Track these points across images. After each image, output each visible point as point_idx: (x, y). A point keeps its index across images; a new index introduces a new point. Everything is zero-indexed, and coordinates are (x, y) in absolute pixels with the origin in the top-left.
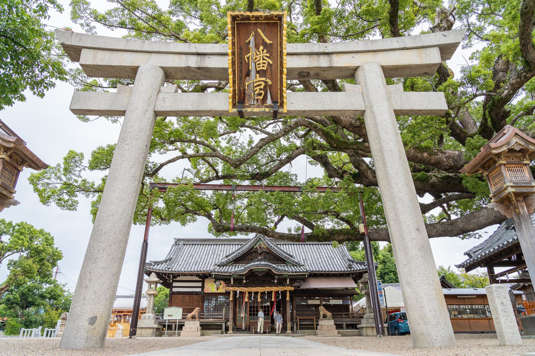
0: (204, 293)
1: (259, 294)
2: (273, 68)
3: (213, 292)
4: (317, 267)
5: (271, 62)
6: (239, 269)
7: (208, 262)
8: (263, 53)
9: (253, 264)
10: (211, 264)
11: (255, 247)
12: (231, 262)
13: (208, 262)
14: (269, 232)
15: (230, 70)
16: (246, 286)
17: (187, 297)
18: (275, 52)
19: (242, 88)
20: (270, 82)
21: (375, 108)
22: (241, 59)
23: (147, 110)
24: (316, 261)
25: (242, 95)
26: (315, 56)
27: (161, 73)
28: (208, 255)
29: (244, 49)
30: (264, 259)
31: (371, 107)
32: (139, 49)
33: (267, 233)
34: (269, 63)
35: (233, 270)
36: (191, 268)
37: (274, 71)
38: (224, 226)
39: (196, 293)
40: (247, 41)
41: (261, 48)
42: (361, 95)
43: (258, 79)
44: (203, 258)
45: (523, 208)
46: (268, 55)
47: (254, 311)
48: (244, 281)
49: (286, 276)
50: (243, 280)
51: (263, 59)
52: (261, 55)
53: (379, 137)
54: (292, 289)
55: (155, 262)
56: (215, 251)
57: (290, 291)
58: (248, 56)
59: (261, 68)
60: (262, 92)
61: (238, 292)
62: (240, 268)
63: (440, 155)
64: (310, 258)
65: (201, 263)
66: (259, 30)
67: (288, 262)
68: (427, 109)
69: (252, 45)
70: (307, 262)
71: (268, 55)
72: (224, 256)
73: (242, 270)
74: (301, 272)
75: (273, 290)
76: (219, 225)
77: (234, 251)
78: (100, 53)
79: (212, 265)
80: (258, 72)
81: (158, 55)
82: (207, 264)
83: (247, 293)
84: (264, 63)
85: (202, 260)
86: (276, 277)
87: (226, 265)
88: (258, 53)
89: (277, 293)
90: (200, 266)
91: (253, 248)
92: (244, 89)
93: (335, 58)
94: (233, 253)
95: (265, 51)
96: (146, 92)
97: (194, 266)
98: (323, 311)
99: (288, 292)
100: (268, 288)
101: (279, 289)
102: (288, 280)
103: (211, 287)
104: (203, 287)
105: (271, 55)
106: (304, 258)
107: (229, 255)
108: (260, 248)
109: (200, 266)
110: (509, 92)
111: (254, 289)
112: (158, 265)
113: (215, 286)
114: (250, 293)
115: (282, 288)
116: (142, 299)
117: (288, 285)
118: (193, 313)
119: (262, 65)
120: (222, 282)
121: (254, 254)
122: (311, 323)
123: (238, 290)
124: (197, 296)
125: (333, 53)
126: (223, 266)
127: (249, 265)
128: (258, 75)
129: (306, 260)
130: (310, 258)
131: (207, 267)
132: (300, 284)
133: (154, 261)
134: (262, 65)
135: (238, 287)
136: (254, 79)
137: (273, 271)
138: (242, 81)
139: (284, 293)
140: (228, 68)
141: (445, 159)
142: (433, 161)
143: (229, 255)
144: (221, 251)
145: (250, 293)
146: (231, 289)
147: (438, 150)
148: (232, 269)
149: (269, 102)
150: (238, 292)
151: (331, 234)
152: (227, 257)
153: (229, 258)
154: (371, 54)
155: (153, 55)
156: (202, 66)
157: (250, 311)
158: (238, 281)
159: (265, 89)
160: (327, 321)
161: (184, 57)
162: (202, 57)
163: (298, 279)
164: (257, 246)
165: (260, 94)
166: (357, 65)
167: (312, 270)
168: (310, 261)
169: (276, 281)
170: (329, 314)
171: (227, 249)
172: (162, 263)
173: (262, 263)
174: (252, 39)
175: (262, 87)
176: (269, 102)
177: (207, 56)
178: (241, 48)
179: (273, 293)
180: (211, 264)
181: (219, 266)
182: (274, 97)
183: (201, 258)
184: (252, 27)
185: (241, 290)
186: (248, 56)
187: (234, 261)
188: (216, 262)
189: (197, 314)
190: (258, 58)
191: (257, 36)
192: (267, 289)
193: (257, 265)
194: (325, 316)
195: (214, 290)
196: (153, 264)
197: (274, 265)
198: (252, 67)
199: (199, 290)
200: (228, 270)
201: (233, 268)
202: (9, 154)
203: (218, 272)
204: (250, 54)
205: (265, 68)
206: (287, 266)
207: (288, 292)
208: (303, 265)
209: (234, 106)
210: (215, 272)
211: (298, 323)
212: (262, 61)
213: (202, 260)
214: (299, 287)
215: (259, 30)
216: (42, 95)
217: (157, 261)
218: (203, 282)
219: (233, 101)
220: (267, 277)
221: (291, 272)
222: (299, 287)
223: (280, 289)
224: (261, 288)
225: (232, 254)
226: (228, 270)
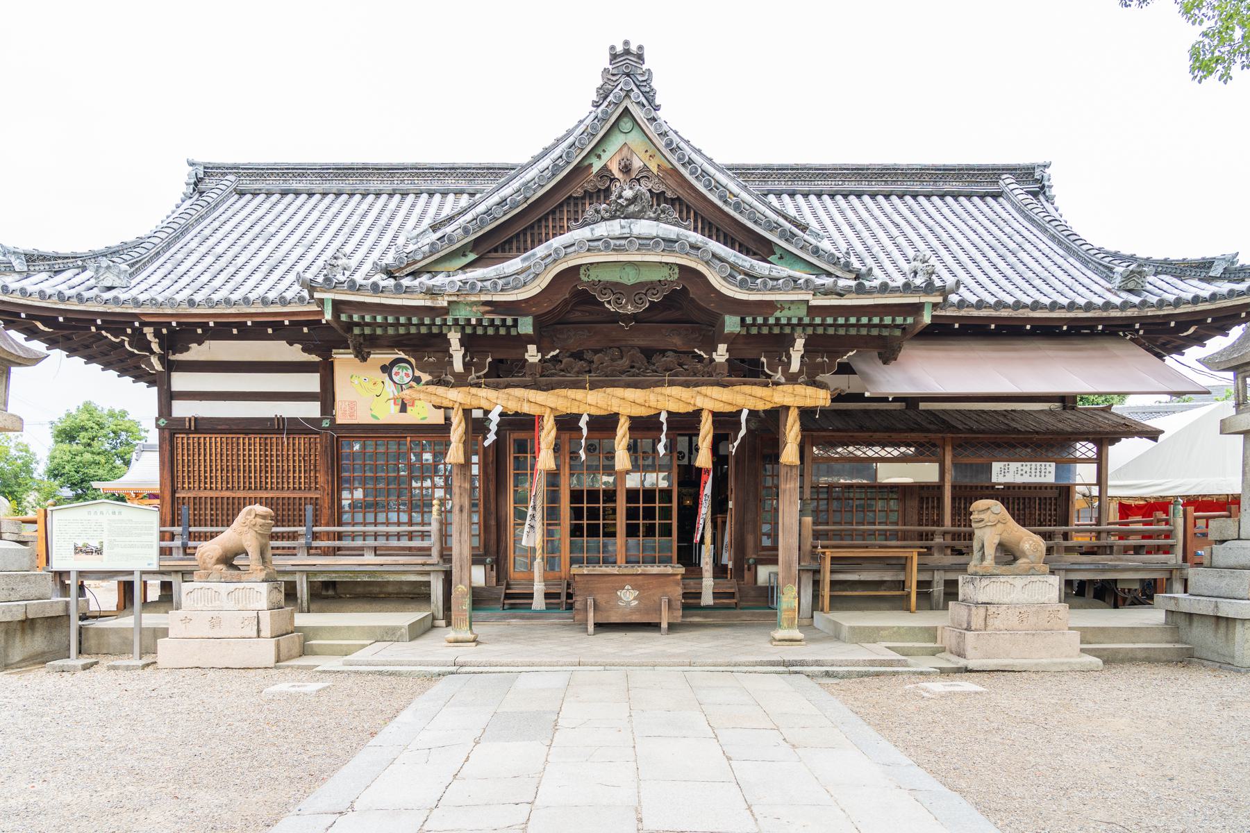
0: (335, 427)
1: (623, 428)
11: (597, 166)
12: (461, 252)
16: (544, 379)
17: (253, 446)
39: (294, 427)
47: (593, 514)
48: (532, 355)
54: (819, 398)
55: (31, 258)
57: (806, 414)
64: (890, 247)
86: (732, 324)
89: (725, 422)
91: (580, 170)
98: (992, 522)
100: (676, 391)
102: (800, 343)
103: (369, 393)
104: (326, 397)
108: (626, 169)
111: (589, 402)
114: (567, 423)
115: (759, 391)
116: (157, 442)
117: (792, 379)
118: (228, 536)
122: (888, 576)
123: (497, 402)
124: (301, 441)
130: (890, 247)
133: (27, 246)
137: (715, 280)
139: (768, 424)
145: (567, 423)
150: (494, 417)
152: (434, 228)
153: (448, 230)
157: (577, 514)
158: (495, 355)
160: (1019, 581)
164: (610, 158)
169: (721, 354)
170: (1030, 542)
172: (79, 261)
173: (644, 227)
185: (513, 407)
187: (476, 244)
189: (251, 542)
192: (669, 399)
193: (607, 244)
194: (1008, 554)
195: (388, 414)
196: (19, 265)
199: (312, 410)
202: (583, 423)
207: (793, 416)
211: (827, 577)
217: (47, 248)
218: (327, 371)
220: (675, 325)
223: (746, 398)
224: (631, 394)
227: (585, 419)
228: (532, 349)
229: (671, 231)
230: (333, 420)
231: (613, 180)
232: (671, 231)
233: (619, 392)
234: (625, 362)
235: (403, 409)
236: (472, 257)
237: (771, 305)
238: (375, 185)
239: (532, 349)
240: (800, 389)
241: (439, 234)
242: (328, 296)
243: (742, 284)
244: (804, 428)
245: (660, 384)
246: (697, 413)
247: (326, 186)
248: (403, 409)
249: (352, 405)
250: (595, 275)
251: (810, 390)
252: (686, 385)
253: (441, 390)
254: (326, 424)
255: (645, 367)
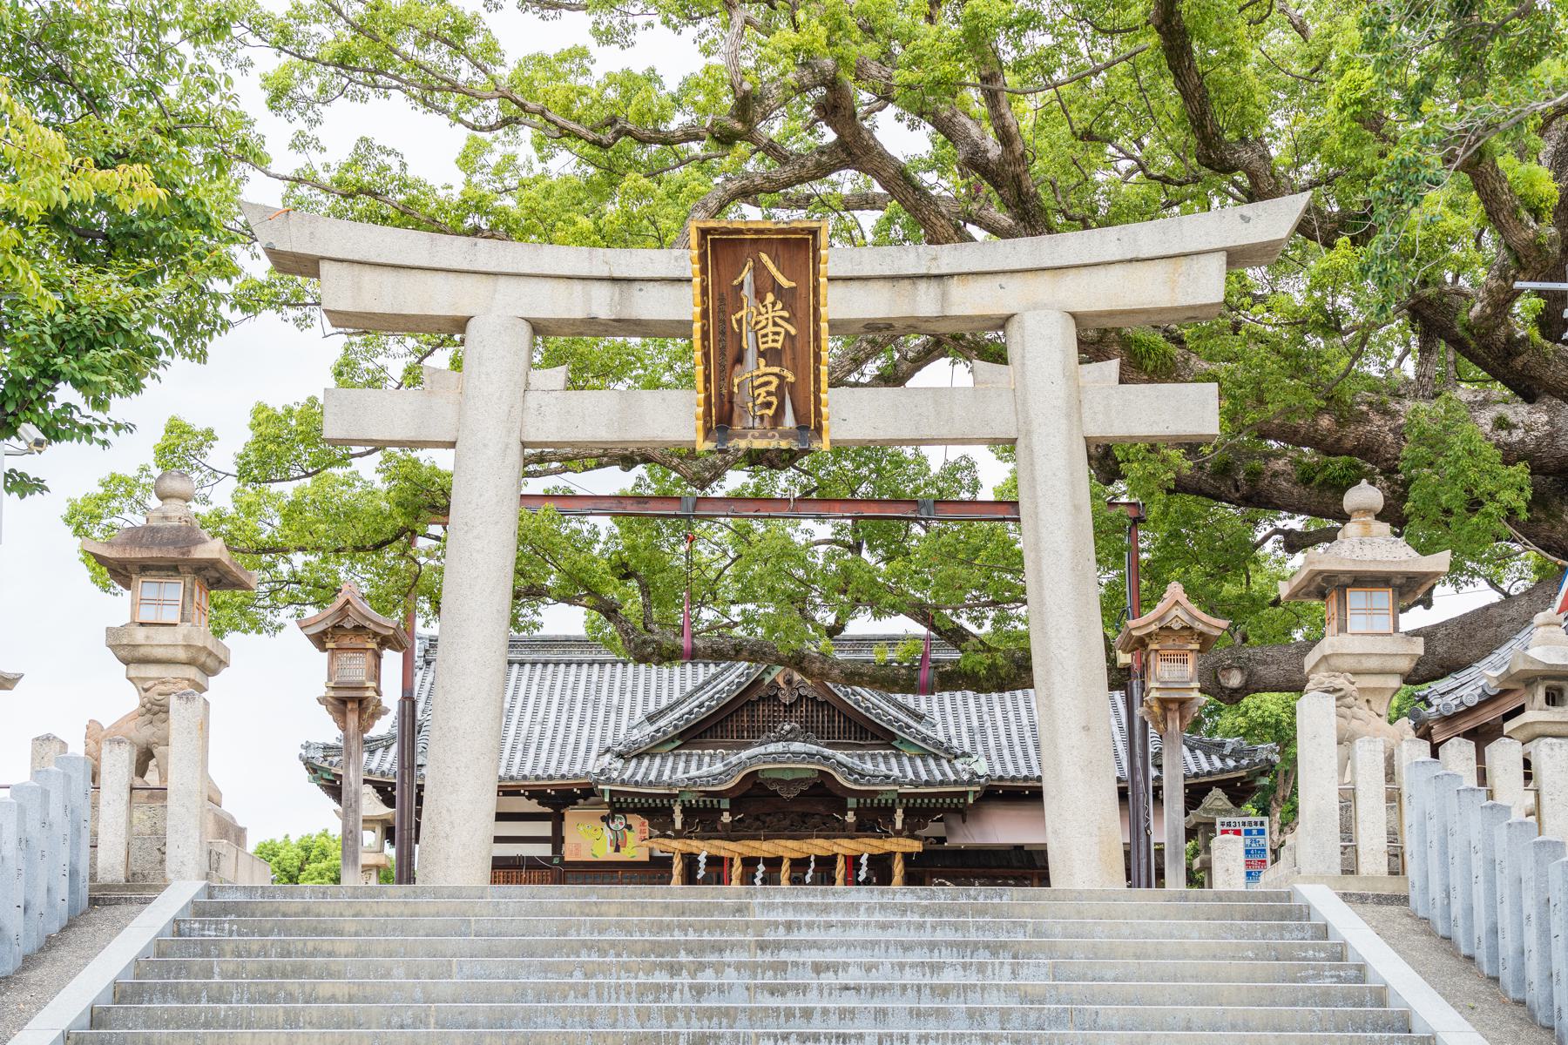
0: (563, 863)
1: (785, 866)
2: (798, 345)
3: (601, 858)
4: (1022, 762)
5: (793, 331)
6: (705, 770)
7: (572, 739)
8: (772, 310)
9: (762, 750)
10: (588, 750)
11: (768, 680)
12: (672, 740)
13: (572, 739)
14: (812, 661)
15: (697, 326)
16: (732, 833)
18: (800, 303)
19: (724, 391)
20: (791, 378)
21: (1035, 438)
22: (723, 323)
23: (507, 446)
24: (1022, 739)
25: (727, 407)
26: (906, 282)
27: (526, 330)
28: (571, 709)
29: (729, 300)
30: (809, 730)
31: (1028, 433)
32: (466, 267)
33: (805, 664)
34: (787, 333)
35: (679, 775)
36: (509, 766)
37: (794, 353)
38: (659, 644)
40: (735, 282)
41: (770, 297)
42: (1011, 394)
43: (763, 369)
44: (551, 724)
45: (1174, 721)
46: (786, 314)
48: (726, 818)
49: (890, 797)
50: (721, 812)
51: (775, 324)
52: (770, 315)
53: (1037, 514)
54: (916, 846)
56: (598, 691)
57: (907, 856)
58: (738, 316)
59: (771, 345)
60: (774, 399)
61: (702, 859)
62: (710, 768)
63: (1377, 420)
64: (1000, 724)
65: (546, 745)
66: (764, 257)
67: (903, 741)
68: (1167, 432)
69: (748, 292)
70: (985, 743)
71: (786, 314)
72: (639, 715)
73: (715, 777)
74: (949, 784)
75: (841, 851)
76: (644, 642)
77: (677, 695)
78: (368, 275)
79: (593, 754)
80: (762, 354)
81: (513, 281)
82: (569, 749)
83: (737, 863)
84: (777, 334)
85: (549, 733)
86: (852, 802)
87: (650, 753)
88: (763, 310)
90: (544, 756)
92: (731, 394)
93: (955, 288)
94: (678, 703)
95: (779, 305)
96: (500, 398)
97: (519, 755)
99: (898, 857)
100: (820, 842)
101: (862, 848)
102: (900, 812)
104: (557, 840)
105: (793, 314)
106: (975, 723)
107: (661, 713)
109: (544, 756)
110: (1483, 310)
112: (372, 752)
113: (607, 835)
115: (874, 842)
117: (898, 834)
119: (771, 337)
120: (636, 820)
121: (763, 711)
125: (952, 275)
126: (640, 756)
127: (744, 754)
128: (762, 361)
129: (983, 732)
131: (572, 762)
132: (948, 828)
134: (771, 337)
135: (702, 839)
136: (754, 369)
138: (724, 374)
140: (690, 323)
141: (1390, 438)
142: (1349, 443)
143: (661, 713)
144: (622, 693)
146: (677, 846)
147: (1370, 404)
148: (674, 770)
149: (789, 421)
150: (702, 859)
151: (1019, 667)
152: (651, 719)
153: (662, 723)
154: (1047, 276)
155: (502, 280)
156: (622, 317)
159: (779, 392)
161: (578, 287)
162: (625, 285)
163: (936, 810)
165: (768, 405)
166: (1006, 311)
167: (999, 771)
168: (997, 737)
171: (648, 680)
173: (797, 746)
174: (747, 276)
175: (772, 388)
176: (789, 421)
177: (637, 285)
178: (721, 299)
179: (840, 864)
180: (588, 750)
181: (620, 755)
182: (802, 411)
183: (544, 722)
184: (747, 249)
185: (714, 852)
186: (738, 316)
187: (681, 735)
188: (609, 742)
190: (763, 322)
191: (759, 269)
197: (840, 756)
198: (748, 342)
199: (545, 850)
200: (660, 773)
201: (681, 765)
203: (623, 783)
204: (744, 313)
205: (779, 345)
206: (898, 757)
207: (898, 857)
208: (964, 754)
209: (708, 433)
210: (609, 781)
212: (770, 328)
213: (549, 733)
214: (942, 840)
215: (764, 257)
216: (202, 357)
218: (558, 820)
219: (705, 422)
221: (911, 783)
222: (942, 840)
224: (791, 844)
225: (671, 708)
226: (660, 773)
227: (866, 856)
228: (726, 814)
229: (814, 748)
230: (562, 858)
231: (779, 689)
232: (814, 748)
233: (783, 842)
234: (788, 822)
235: (617, 849)
236: (678, 743)
237: (876, 792)
238: (577, 655)
239: (726, 814)
240: (901, 840)
241: (655, 727)
242: (607, 787)
243: (856, 781)
244: (906, 865)
245: (810, 837)
246: (836, 855)
247: (534, 657)
248: (617, 849)
249: (578, 846)
250: (766, 775)
251: (909, 842)
252: (827, 838)
253: (667, 841)
254: (556, 861)
255: (798, 827)
